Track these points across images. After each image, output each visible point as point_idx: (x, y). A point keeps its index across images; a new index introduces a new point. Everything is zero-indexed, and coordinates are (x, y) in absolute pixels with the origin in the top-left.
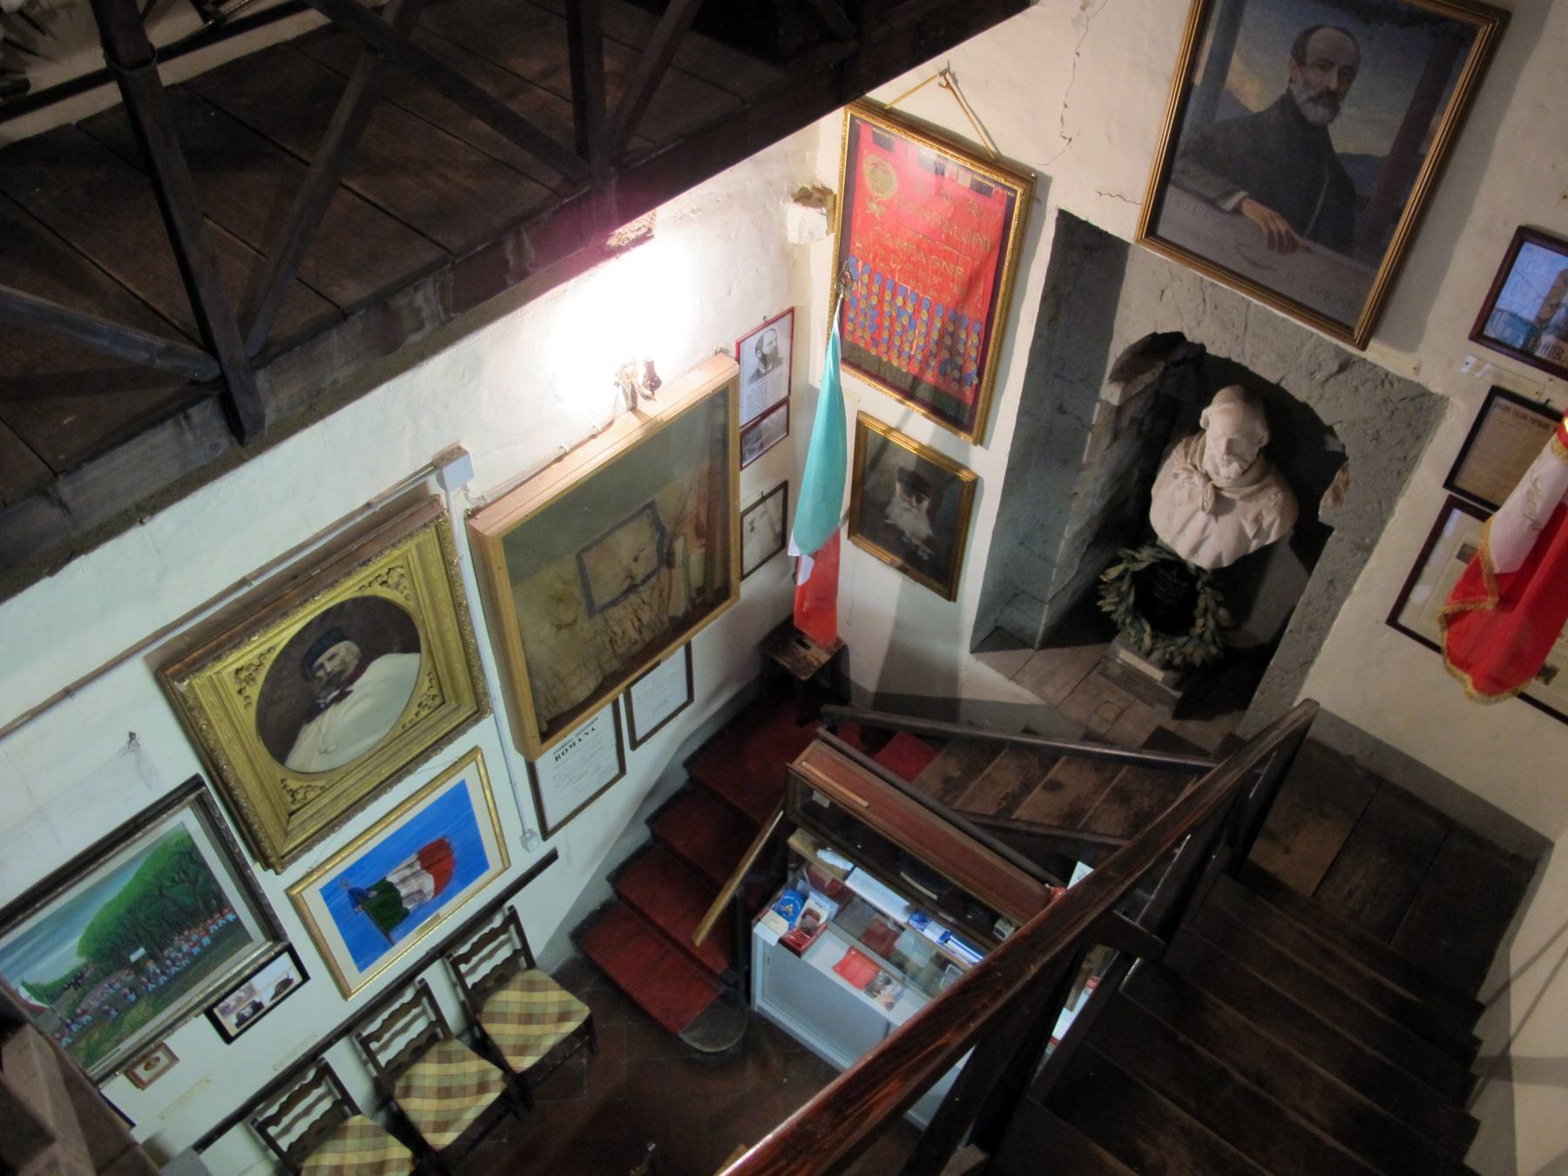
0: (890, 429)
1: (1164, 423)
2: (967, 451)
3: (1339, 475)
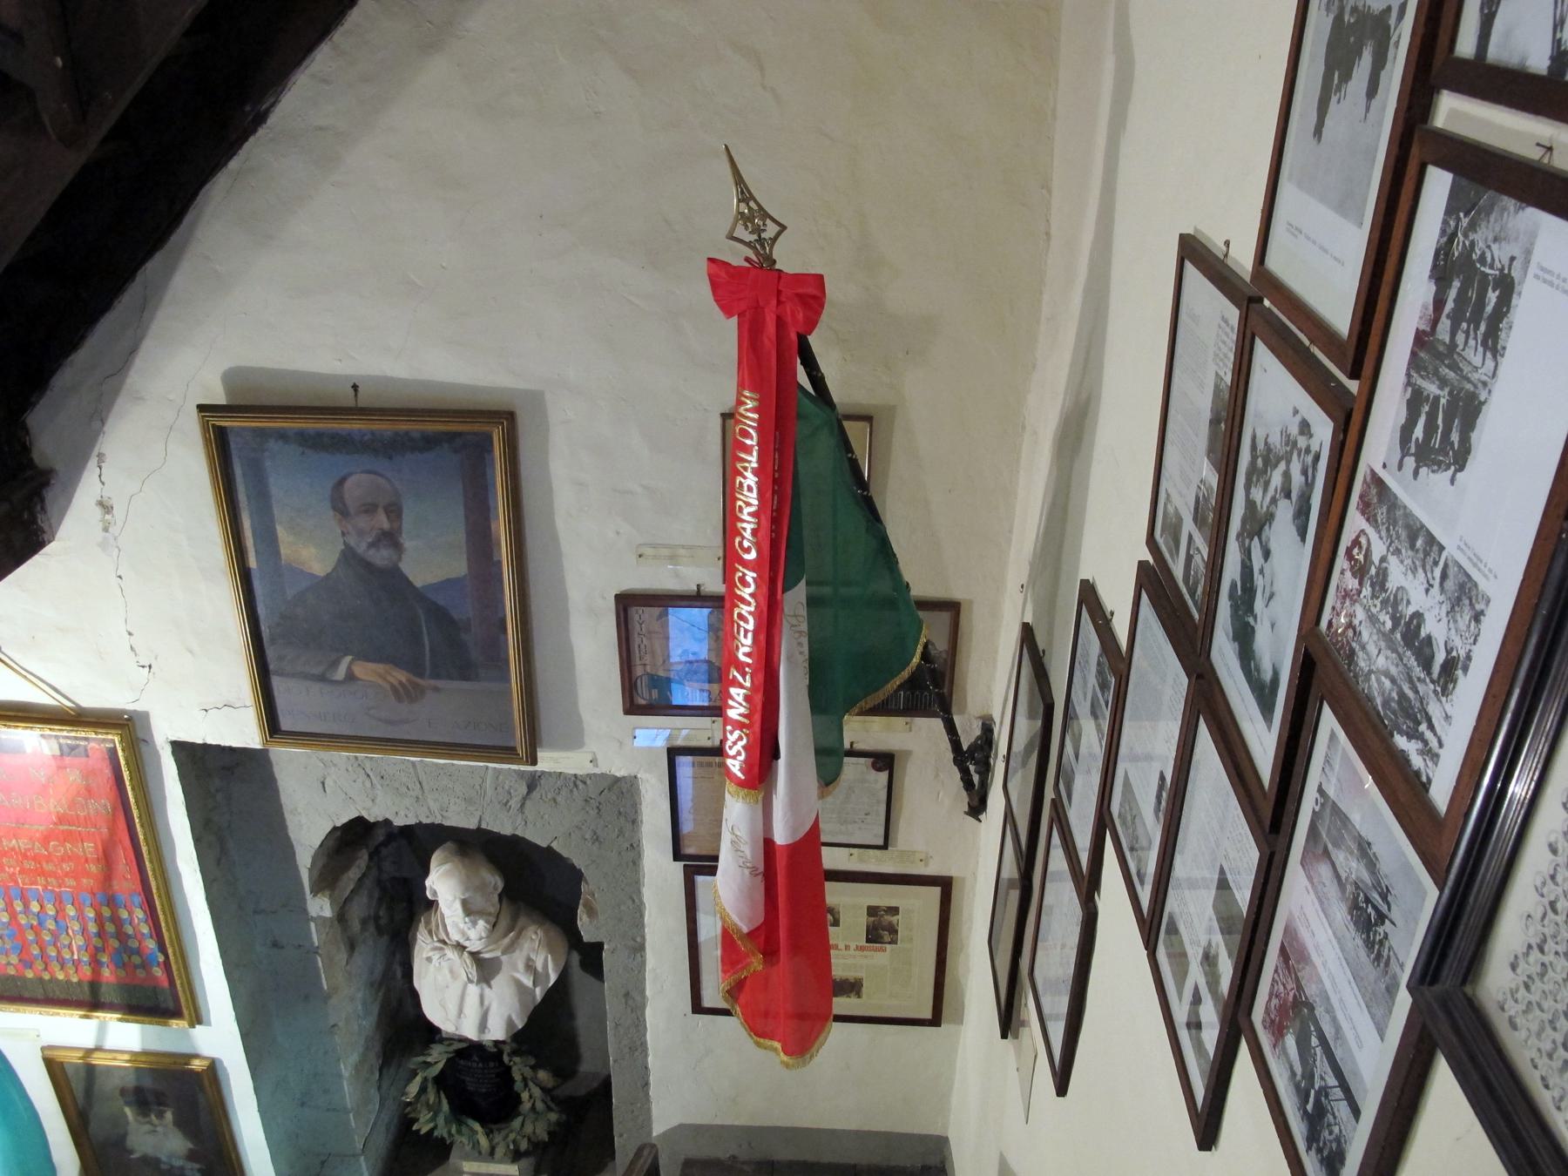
0: (89, 1052)
1: (403, 909)
2: (189, 1037)
3: (583, 887)
